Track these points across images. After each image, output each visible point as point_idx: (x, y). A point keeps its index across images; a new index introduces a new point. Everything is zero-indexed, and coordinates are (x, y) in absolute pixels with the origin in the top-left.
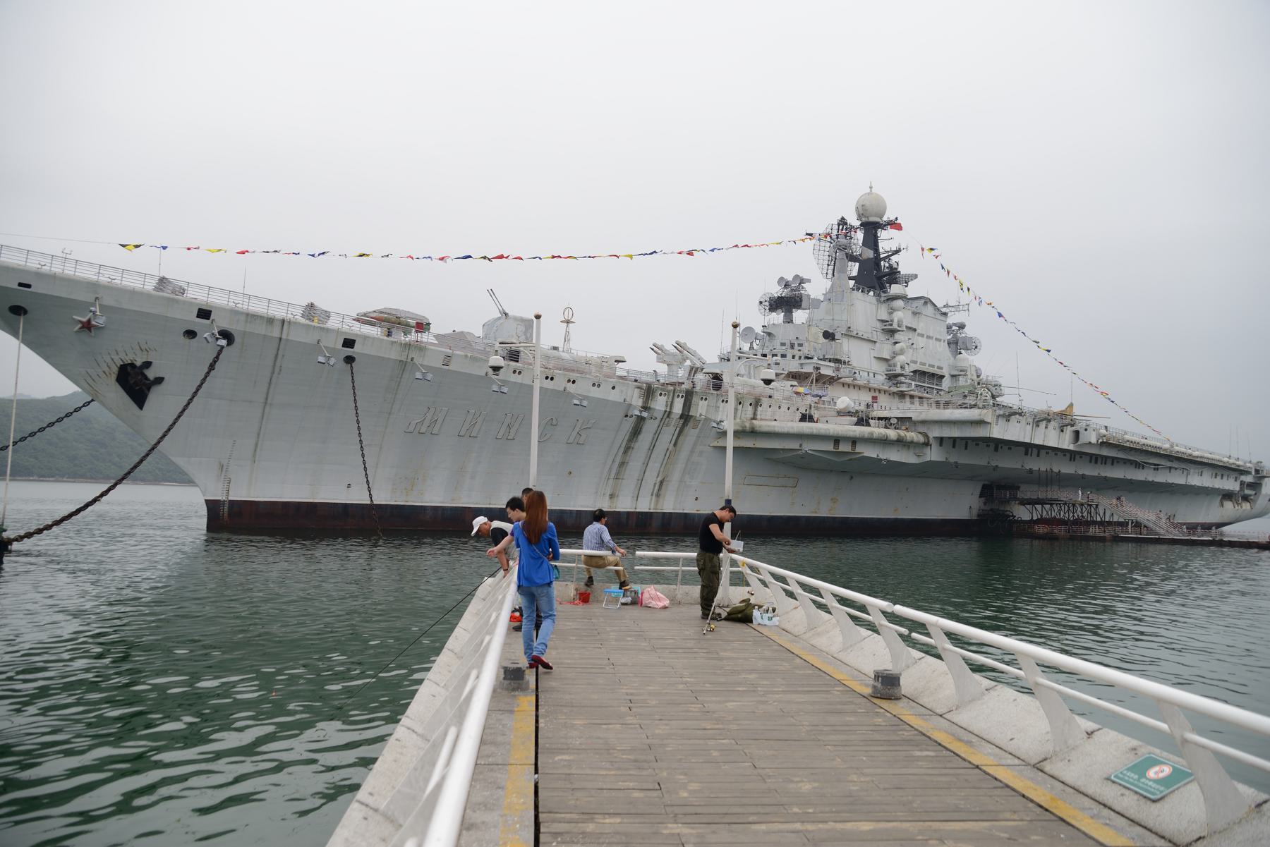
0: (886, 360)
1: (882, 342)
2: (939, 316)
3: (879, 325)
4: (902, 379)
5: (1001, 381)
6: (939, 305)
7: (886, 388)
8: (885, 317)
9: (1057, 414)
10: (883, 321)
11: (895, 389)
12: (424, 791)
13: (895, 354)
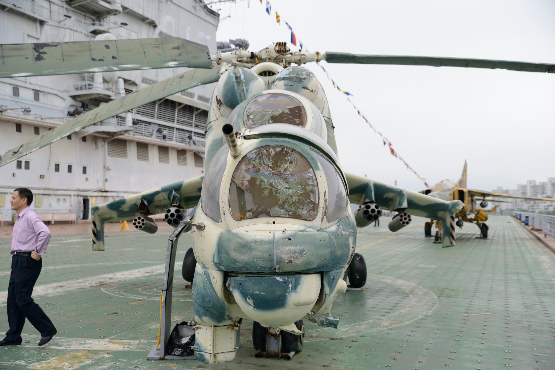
2: (202, 13)
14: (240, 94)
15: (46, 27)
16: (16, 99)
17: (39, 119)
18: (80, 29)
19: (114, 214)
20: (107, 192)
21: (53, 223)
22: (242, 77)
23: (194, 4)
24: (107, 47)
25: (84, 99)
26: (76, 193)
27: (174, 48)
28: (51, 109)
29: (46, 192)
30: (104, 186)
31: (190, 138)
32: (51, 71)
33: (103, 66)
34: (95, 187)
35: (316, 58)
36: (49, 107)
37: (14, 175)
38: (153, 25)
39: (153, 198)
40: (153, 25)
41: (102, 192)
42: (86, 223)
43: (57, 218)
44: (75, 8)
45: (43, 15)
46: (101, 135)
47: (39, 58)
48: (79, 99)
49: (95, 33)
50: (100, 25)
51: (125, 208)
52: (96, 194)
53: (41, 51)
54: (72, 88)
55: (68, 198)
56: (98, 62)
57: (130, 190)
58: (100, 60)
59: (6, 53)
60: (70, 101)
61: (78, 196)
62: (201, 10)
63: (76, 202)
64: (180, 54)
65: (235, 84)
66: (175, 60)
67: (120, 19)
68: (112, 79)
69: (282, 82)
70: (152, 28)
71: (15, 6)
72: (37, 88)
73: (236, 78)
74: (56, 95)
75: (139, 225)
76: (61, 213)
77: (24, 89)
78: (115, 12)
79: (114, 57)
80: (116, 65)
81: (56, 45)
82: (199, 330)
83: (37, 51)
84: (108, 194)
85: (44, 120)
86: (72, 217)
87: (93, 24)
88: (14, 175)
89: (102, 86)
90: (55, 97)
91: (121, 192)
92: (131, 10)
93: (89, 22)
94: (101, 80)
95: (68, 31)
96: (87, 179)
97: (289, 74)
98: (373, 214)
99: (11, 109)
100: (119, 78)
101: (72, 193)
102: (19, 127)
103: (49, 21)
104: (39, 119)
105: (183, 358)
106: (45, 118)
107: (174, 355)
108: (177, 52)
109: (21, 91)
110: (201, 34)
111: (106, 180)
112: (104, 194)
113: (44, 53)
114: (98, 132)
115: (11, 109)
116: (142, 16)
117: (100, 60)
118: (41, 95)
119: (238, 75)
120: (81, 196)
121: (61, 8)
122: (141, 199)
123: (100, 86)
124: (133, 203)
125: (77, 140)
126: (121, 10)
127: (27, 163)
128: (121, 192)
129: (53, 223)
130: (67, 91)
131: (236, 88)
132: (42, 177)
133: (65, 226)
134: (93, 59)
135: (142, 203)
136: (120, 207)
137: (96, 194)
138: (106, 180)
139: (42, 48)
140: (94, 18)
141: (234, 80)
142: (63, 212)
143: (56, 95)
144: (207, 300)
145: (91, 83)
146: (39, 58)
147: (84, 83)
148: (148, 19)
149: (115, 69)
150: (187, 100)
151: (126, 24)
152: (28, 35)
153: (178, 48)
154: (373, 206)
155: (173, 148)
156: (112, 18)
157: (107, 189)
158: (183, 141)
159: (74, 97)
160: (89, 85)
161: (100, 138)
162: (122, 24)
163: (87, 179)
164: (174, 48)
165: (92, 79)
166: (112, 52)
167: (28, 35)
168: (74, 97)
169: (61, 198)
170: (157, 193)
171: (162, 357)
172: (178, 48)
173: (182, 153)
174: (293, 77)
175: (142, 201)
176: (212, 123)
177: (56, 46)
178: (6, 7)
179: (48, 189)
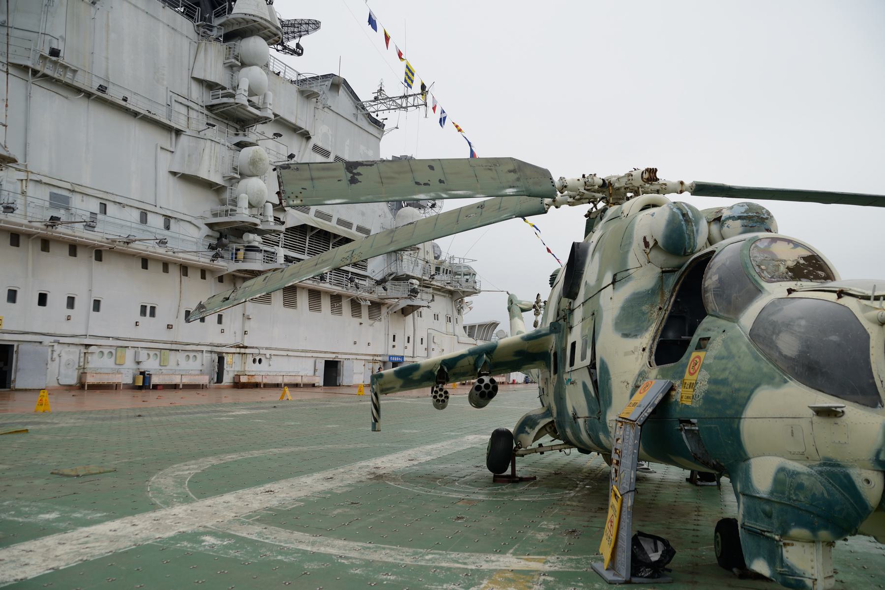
0: (209, 185)
1: (198, 136)
2: (364, 123)
3: (197, 93)
4: (255, 239)
5: (475, 267)
6: (365, 95)
7: (204, 260)
8: (216, 72)
9: (229, 275)
10: (211, 86)
11: (227, 266)
12: (481, 206)
13: (240, 174)
14: (689, 235)
15: (183, 139)
16: (143, 227)
17: (171, 253)
18: (222, 141)
19: (400, 382)
20: (246, 347)
21: (181, 386)
22: (690, 214)
23: (354, 111)
24: (431, 168)
25: (222, 228)
26: (209, 348)
27: (510, 171)
28: (183, 240)
29: (174, 347)
30: (243, 340)
31: (351, 280)
32: (370, 197)
33: (430, 192)
34: (232, 341)
35: (679, 189)
36: (181, 236)
37: (137, 324)
38: (306, 136)
39: (455, 364)
40: (306, 136)
41: (240, 347)
42: (219, 388)
43: (186, 380)
44: (216, 114)
45: (179, 122)
46: (242, 275)
47: (353, 181)
48: (216, 228)
49: (241, 145)
50: (245, 135)
51: (416, 375)
52: (233, 350)
53: (355, 171)
54: (208, 215)
55: (199, 355)
56: (423, 187)
57: (274, 346)
58: (425, 184)
59: (315, 174)
60: (206, 230)
61: (211, 352)
62: (364, 119)
63: (207, 360)
64: (518, 179)
65: (683, 222)
66: (513, 187)
67: (269, 130)
68: (259, 203)
69: (739, 222)
70: (304, 141)
71: (150, 112)
72: (169, 214)
73: (684, 215)
74: (190, 222)
75: (441, 399)
76: (191, 375)
77: (153, 215)
78: (265, 120)
79: (441, 181)
80: (446, 190)
81: (370, 164)
82: (789, 548)
83: (351, 172)
84: (247, 351)
85: (176, 254)
86: (204, 380)
87: (237, 135)
88: (137, 324)
89: (247, 212)
90: (188, 224)
91: (262, 348)
92: (281, 118)
93: (232, 131)
94: (247, 205)
95: (209, 142)
96: (222, 331)
97: (745, 212)
98: (490, 389)
99: (140, 240)
100: (267, 202)
101: (205, 348)
102: (145, 262)
103: (187, 130)
104: (171, 253)
105: (655, 580)
106: (178, 252)
107: (641, 577)
108: (513, 176)
109: (150, 217)
110: (362, 148)
111: (245, 333)
112: (243, 351)
113: (359, 174)
114: (239, 271)
115: (140, 240)
116: (294, 125)
117: (425, 184)
118: (172, 221)
119: (685, 212)
120: (215, 352)
121: (200, 115)
122: (441, 364)
123: (244, 211)
124: (429, 369)
125: (213, 280)
126: (272, 117)
127: (153, 309)
128: (262, 348)
129: (181, 386)
130: (202, 218)
131: (684, 227)
132: (169, 327)
133: (201, 392)
134: (417, 183)
135: (441, 370)
136: (411, 374)
137: (233, 350)
138: (245, 333)
139: (356, 168)
140: (238, 127)
141: (681, 217)
142: (193, 372)
143: (190, 222)
144: (837, 508)
145: (234, 208)
146: (353, 181)
147: (224, 208)
148: (301, 129)
149: (444, 196)
150: (345, 231)
151: (280, 135)
152: (161, 148)
153: (514, 171)
154: (486, 379)
155: (326, 293)
156: (259, 127)
157: (246, 344)
158: (339, 284)
159: (211, 226)
160: (232, 210)
161: (240, 277)
162: (275, 134)
163: (222, 331)
164: (510, 171)
165: (234, 202)
166: (437, 174)
167: (161, 148)
168: (211, 226)
169: (191, 355)
170: (462, 357)
171: (628, 579)
172: (514, 171)
173: (336, 299)
174: (753, 217)
175: (441, 367)
176: (631, 271)
177: (371, 165)
178: (140, 113)
179: (176, 343)
